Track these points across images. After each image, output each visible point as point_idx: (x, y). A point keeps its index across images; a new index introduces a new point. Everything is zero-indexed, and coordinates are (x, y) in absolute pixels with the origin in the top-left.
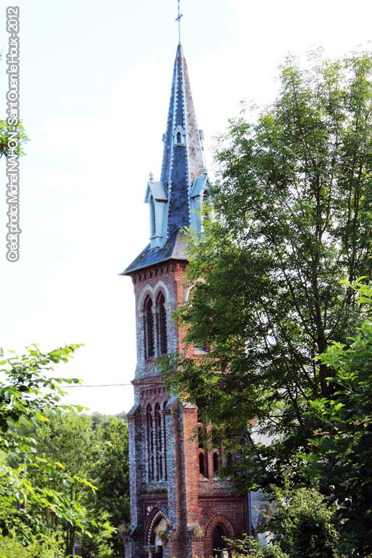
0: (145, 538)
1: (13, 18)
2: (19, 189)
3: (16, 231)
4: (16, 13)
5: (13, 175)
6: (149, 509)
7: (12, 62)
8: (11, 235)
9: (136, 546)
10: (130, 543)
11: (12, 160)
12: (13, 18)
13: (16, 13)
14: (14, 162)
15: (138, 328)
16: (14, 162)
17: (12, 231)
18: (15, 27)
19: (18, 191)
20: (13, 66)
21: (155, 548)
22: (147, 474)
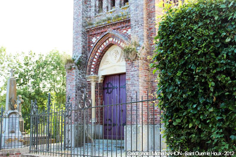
0: (88, 68)
1: (230, 154)
2: (158, 156)
3: (140, 155)
4: (232, 155)
5: (164, 153)
6: (94, 40)
7: (212, 153)
8: (138, 153)
9: (80, 74)
10: (74, 71)
11: (170, 153)
12: (230, 154)
13: (232, 155)
14: (169, 154)
15: (75, 13)
16: (169, 154)
17: (140, 153)
18: (226, 154)
19: (157, 156)
20: (210, 154)
21: (98, 78)
22: (93, 8)
